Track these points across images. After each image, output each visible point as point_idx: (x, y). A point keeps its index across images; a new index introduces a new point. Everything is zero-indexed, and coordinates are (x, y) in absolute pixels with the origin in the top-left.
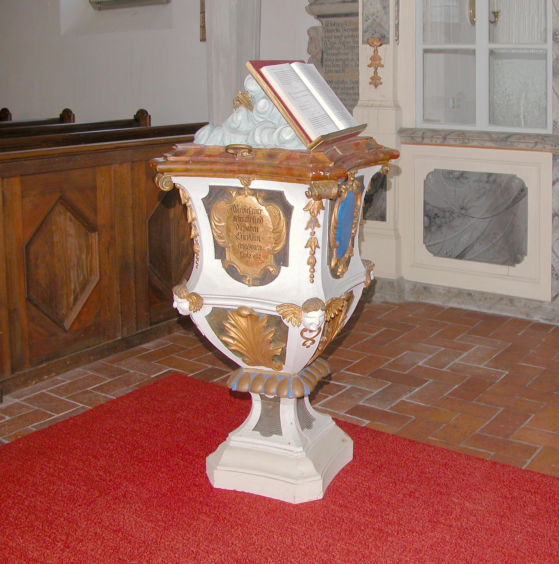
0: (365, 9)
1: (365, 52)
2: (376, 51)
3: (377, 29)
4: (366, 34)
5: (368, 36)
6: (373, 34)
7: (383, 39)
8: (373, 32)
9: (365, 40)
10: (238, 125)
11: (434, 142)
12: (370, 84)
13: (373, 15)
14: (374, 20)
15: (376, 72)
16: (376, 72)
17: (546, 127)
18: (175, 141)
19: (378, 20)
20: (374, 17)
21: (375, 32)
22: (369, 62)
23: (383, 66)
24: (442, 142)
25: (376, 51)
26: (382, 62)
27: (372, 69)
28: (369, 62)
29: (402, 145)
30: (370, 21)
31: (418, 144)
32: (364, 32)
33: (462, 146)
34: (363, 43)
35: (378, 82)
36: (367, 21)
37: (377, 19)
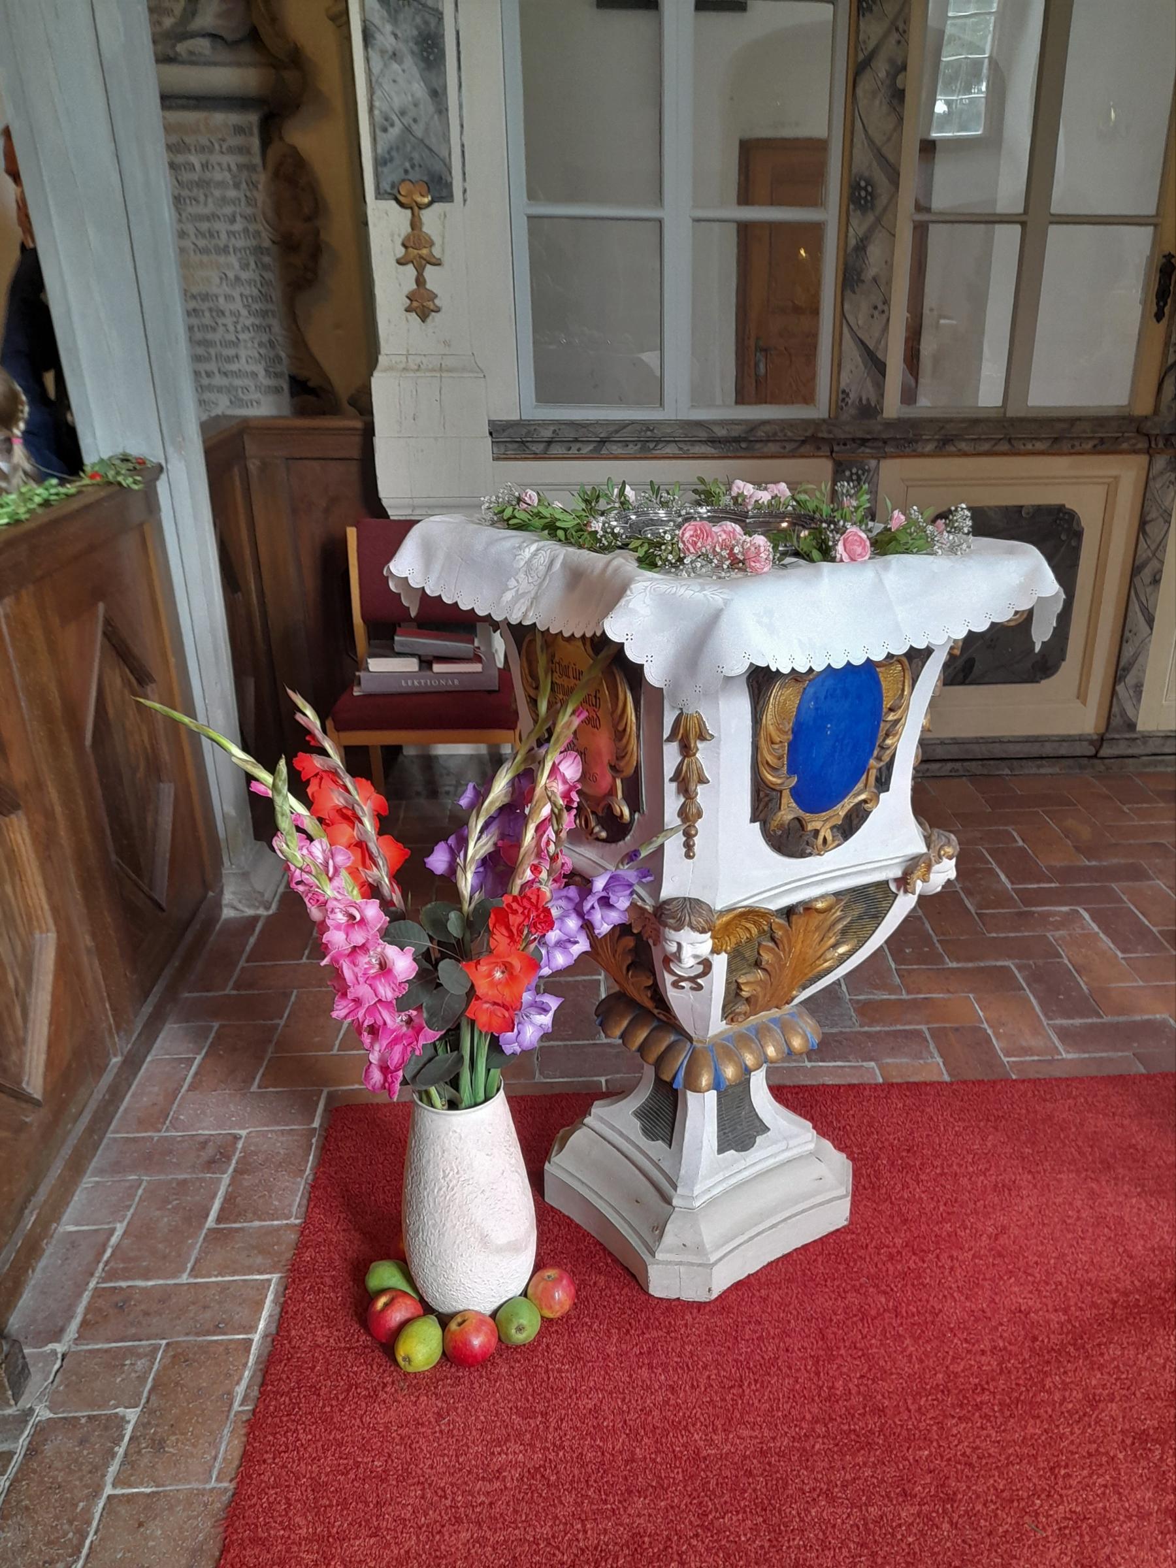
0: (378, 93)
1: (386, 224)
2: (415, 224)
3: (416, 155)
4: (386, 170)
5: (391, 175)
6: (406, 172)
7: (439, 188)
8: (407, 165)
9: (386, 186)
10: (754, 986)
11: (1078, 448)
12: (408, 310)
13: (403, 113)
14: (408, 129)
15: (420, 281)
16: (420, 281)
17: (808, 398)
18: (842, 244)
19: (418, 130)
20: (407, 120)
21: (413, 167)
22: (401, 252)
23: (437, 263)
24: (594, 450)
25: (415, 224)
26: (436, 252)
27: (410, 271)
28: (401, 252)
29: (90, 458)
30: (395, 132)
31: (537, 457)
32: (380, 163)
33: (1049, 454)
34: (379, 195)
35: (431, 305)
36: (385, 130)
37: (414, 127)
